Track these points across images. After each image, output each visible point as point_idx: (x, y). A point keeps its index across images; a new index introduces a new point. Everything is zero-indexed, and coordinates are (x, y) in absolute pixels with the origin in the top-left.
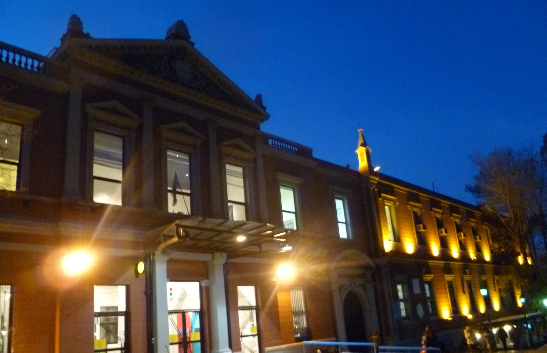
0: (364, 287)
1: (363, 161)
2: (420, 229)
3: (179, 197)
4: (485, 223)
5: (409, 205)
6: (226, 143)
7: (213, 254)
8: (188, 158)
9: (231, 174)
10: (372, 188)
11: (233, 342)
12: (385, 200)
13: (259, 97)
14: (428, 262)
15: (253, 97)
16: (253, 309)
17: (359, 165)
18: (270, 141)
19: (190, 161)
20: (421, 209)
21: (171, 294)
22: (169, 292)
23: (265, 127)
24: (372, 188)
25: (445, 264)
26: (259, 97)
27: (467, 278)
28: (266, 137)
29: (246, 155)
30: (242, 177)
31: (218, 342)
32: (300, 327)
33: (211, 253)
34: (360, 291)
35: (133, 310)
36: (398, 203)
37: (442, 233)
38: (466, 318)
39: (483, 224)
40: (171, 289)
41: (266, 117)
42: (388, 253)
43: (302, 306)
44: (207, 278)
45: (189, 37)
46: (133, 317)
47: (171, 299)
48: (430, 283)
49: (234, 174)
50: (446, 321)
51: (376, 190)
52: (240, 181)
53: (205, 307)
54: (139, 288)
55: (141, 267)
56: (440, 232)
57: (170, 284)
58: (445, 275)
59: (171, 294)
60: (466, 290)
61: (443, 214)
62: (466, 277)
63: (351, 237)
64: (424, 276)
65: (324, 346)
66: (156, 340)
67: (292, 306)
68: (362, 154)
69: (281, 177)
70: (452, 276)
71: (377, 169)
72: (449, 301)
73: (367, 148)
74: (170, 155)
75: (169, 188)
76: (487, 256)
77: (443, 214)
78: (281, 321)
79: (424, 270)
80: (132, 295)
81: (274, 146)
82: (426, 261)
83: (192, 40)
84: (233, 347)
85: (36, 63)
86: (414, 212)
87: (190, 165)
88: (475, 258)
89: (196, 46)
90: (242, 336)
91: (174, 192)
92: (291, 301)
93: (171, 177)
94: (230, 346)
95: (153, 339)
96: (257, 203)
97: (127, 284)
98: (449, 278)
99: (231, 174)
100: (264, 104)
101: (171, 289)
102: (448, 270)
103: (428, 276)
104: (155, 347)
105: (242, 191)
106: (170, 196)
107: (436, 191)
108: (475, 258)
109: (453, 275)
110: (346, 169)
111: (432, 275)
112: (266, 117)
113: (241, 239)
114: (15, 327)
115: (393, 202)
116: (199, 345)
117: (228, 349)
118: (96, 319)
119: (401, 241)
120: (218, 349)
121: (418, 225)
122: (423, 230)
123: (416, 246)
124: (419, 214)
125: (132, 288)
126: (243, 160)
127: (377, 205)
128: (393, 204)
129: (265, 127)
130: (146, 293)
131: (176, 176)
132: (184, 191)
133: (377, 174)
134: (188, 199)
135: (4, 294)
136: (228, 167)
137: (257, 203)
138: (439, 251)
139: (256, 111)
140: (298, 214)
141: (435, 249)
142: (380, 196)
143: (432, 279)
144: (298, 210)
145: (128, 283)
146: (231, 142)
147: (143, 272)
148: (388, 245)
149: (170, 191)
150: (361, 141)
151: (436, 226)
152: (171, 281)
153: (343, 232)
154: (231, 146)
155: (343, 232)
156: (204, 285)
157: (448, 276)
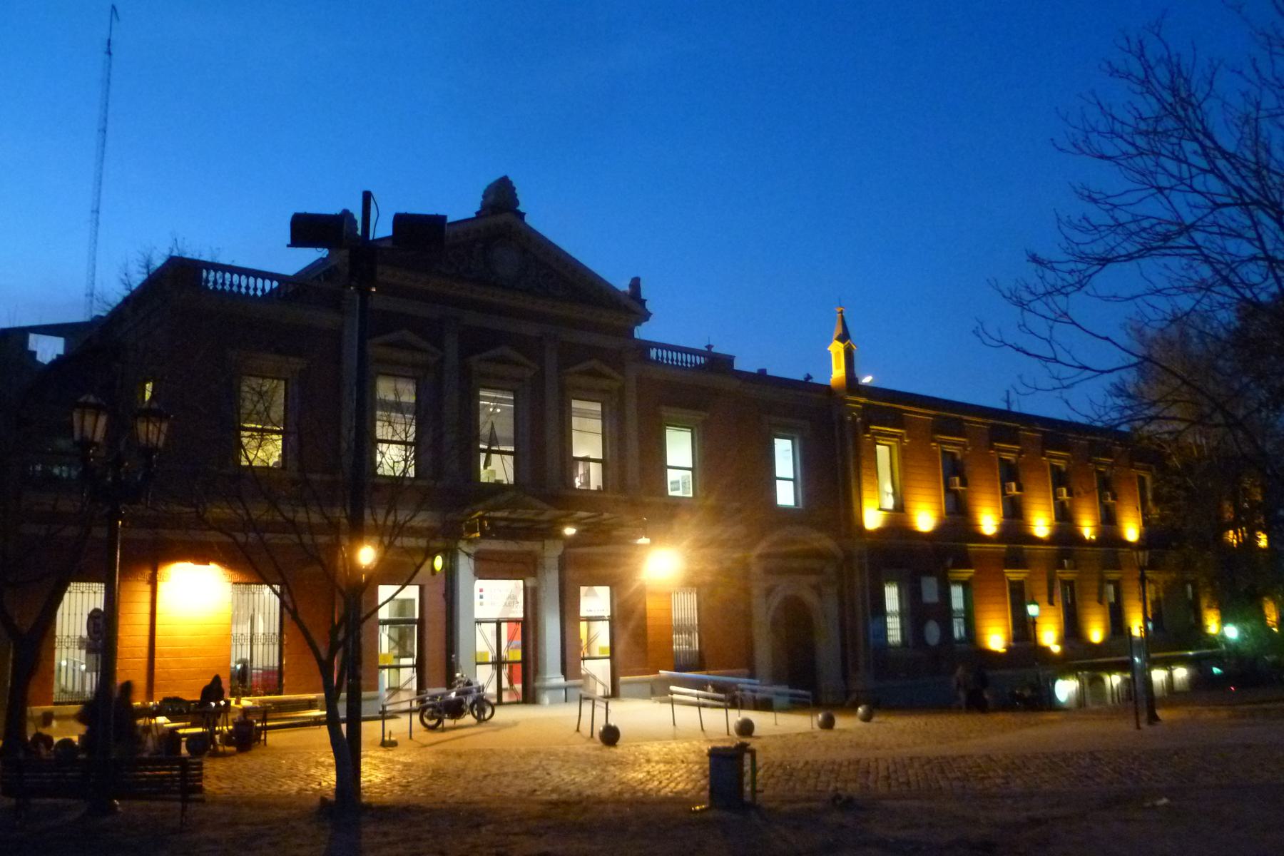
0: (817, 588)
1: (838, 368)
2: (955, 486)
3: (495, 457)
4: (1137, 464)
5: (1044, 455)
6: (572, 370)
7: (544, 541)
8: (512, 398)
9: (587, 416)
10: (849, 418)
11: (568, 668)
12: (876, 437)
13: (636, 283)
14: (967, 547)
15: (623, 286)
16: (606, 620)
17: (832, 374)
18: (653, 353)
19: (515, 402)
20: (963, 446)
21: (481, 597)
22: (477, 594)
23: (643, 332)
24: (849, 418)
25: (1008, 549)
26: (636, 283)
27: (1068, 575)
28: (647, 346)
29: (605, 384)
30: (600, 417)
31: (545, 665)
32: (691, 649)
33: (541, 541)
34: (809, 597)
35: (428, 617)
36: (1072, 462)
37: (1010, 490)
38: (1046, 650)
39: (1132, 466)
40: (481, 590)
41: (646, 316)
42: (871, 533)
43: (694, 619)
44: (534, 574)
45: (517, 203)
46: (429, 627)
47: (481, 604)
48: (966, 585)
49: (585, 414)
50: (994, 655)
51: (859, 419)
52: (597, 425)
53: (529, 614)
54: (438, 589)
55: (438, 563)
56: (1102, 498)
57: (480, 584)
58: (1006, 571)
59: (481, 597)
60: (1058, 598)
61: (1020, 453)
62: (1059, 573)
63: (801, 506)
64: (951, 572)
65: (715, 681)
66: (458, 656)
67: (673, 618)
68: (838, 353)
69: (666, 412)
70: (1075, 573)
71: (867, 380)
72: (1007, 618)
73: (849, 344)
74: (483, 396)
75: (482, 446)
76: (1131, 530)
77: (1020, 453)
78: (650, 639)
79: (950, 563)
80: (427, 596)
81: (660, 359)
82: (964, 544)
83: (521, 208)
84: (568, 673)
85: (268, 283)
86: (1053, 467)
87: (515, 408)
88: (1093, 537)
89: (527, 219)
90: (584, 659)
91: (489, 452)
92: (671, 609)
93: (485, 430)
94: (564, 671)
95: (453, 656)
96: (622, 457)
97: (420, 583)
98: (1013, 575)
99: (587, 416)
100: (644, 295)
101: (481, 590)
102: (1016, 561)
103: (957, 572)
104: (455, 665)
105: (598, 441)
106: (483, 457)
107: (1015, 408)
108: (1093, 537)
109: (1027, 571)
110: (806, 386)
111: (973, 571)
112: (646, 316)
113: (1263, 542)
114: (287, 634)
115: (896, 439)
116: (520, 665)
117: (560, 674)
118: (381, 627)
119: (906, 510)
120: (545, 674)
121: (1059, 489)
122: (959, 488)
123: (940, 518)
124: (959, 457)
125: (427, 589)
126: (603, 391)
127: (857, 448)
128: (897, 442)
129: (643, 332)
130: (445, 595)
131: (493, 428)
132: (502, 448)
133: (870, 391)
134: (509, 460)
135: (81, 594)
136: (576, 404)
137: (622, 457)
138: (997, 525)
139: (628, 310)
140: (697, 471)
141: (988, 520)
142: (867, 431)
143: (971, 578)
144: (697, 465)
145: (423, 583)
146: (582, 367)
147: (442, 568)
148: (873, 516)
149: (483, 451)
150: (838, 331)
151: (1050, 481)
152: (480, 578)
153: (786, 495)
154: (581, 373)
155: (786, 495)
156: (529, 584)
157: (1013, 573)
